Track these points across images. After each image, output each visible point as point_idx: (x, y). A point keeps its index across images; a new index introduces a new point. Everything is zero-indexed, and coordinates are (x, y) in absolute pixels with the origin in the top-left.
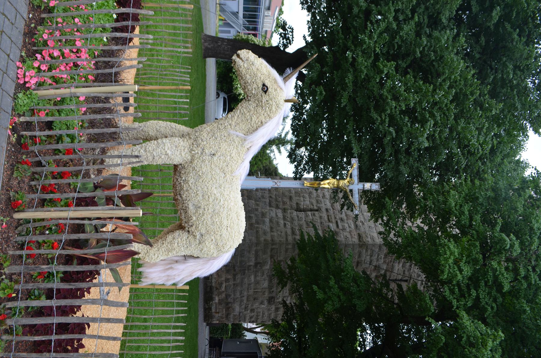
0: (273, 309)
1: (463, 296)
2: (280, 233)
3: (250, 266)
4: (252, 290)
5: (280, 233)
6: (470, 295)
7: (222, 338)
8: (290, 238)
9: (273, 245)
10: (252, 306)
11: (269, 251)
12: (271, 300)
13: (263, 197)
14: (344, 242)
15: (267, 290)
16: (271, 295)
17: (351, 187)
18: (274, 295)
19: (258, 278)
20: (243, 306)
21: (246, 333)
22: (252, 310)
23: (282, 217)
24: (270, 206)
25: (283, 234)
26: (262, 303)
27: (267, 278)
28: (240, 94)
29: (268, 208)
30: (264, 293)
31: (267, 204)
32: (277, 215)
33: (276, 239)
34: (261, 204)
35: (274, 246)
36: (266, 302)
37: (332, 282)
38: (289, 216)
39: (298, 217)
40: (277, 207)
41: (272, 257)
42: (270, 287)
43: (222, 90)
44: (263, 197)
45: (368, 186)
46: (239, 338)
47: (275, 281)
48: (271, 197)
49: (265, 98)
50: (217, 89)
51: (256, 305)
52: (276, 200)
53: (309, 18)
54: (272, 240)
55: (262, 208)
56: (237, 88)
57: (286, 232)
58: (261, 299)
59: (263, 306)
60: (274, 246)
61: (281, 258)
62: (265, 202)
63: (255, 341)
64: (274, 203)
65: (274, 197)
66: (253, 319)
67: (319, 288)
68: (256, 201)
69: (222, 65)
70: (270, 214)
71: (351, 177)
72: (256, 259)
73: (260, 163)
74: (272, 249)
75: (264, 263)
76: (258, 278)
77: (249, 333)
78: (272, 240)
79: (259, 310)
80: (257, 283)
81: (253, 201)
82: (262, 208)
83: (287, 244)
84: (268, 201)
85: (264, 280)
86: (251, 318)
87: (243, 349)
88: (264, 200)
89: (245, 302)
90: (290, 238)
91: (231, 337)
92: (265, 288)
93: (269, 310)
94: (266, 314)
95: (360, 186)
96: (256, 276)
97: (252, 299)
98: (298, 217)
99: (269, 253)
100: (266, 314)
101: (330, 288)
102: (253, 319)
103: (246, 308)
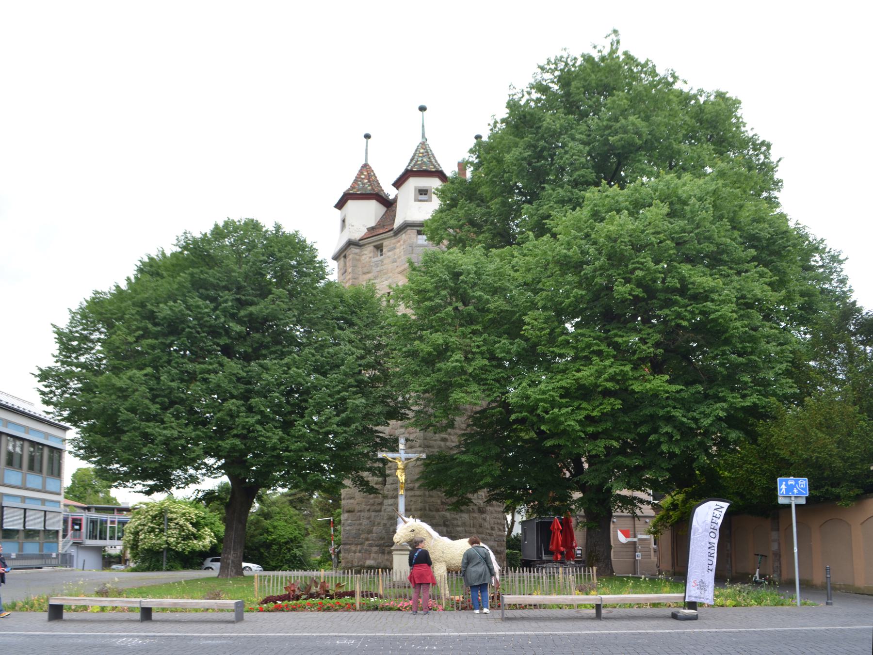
0: (491, 508)
1: (491, 389)
2: (412, 503)
3: (447, 531)
4: (472, 529)
5: (412, 503)
6: (492, 384)
7: (521, 560)
8: (418, 493)
9: (425, 510)
10: (487, 529)
11: (432, 513)
12: (481, 511)
13: (369, 518)
14: (422, 441)
15: (472, 515)
16: (477, 511)
17: (403, 459)
18: (476, 508)
19: (460, 523)
20: (489, 537)
21: (514, 533)
22: (492, 529)
23: (393, 500)
24: (380, 511)
25: (413, 499)
26: (485, 520)
27: (460, 514)
28: (211, 542)
29: (382, 513)
30: (475, 518)
31: (377, 514)
32: (391, 505)
33: (419, 506)
34: (378, 520)
35: (427, 509)
36: (484, 516)
37: (478, 470)
38: (392, 493)
39: (392, 484)
40: (381, 504)
41: (438, 510)
42: (469, 512)
43: (202, 564)
44: (369, 518)
45: (401, 446)
46: (519, 541)
47: (463, 508)
48: (369, 510)
49: (416, 531)
50: (201, 569)
51: (487, 525)
52: (373, 505)
53: (373, 224)
54: (421, 510)
55: (383, 519)
56: (204, 546)
57: (411, 496)
58: (481, 521)
59: (488, 519)
60: (427, 509)
61: (439, 501)
62: (375, 516)
63: (523, 523)
64: (377, 508)
65: (368, 507)
66: (502, 528)
67: (482, 480)
68: (374, 525)
69: (172, 564)
70: (389, 512)
71: (395, 459)
72: (440, 525)
73: (295, 518)
74: (430, 510)
75: (444, 517)
76: (460, 523)
77: (514, 530)
78: (421, 510)
79: (492, 522)
80: (464, 524)
81: (375, 528)
82: (383, 519)
83: (424, 495)
84: (373, 514)
85: (461, 517)
86: (500, 530)
87: (533, 537)
88: (373, 518)
89: (483, 536)
90: (418, 493)
91: (520, 550)
92: (470, 516)
93: (492, 513)
94: (496, 515)
95: (402, 452)
96: (458, 526)
97: (481, 529)
98: (392, 484)
99: (434, 513)
100: (496, 515)
101: (482, 472)
102: (502, 528)
103: (490, 535)
